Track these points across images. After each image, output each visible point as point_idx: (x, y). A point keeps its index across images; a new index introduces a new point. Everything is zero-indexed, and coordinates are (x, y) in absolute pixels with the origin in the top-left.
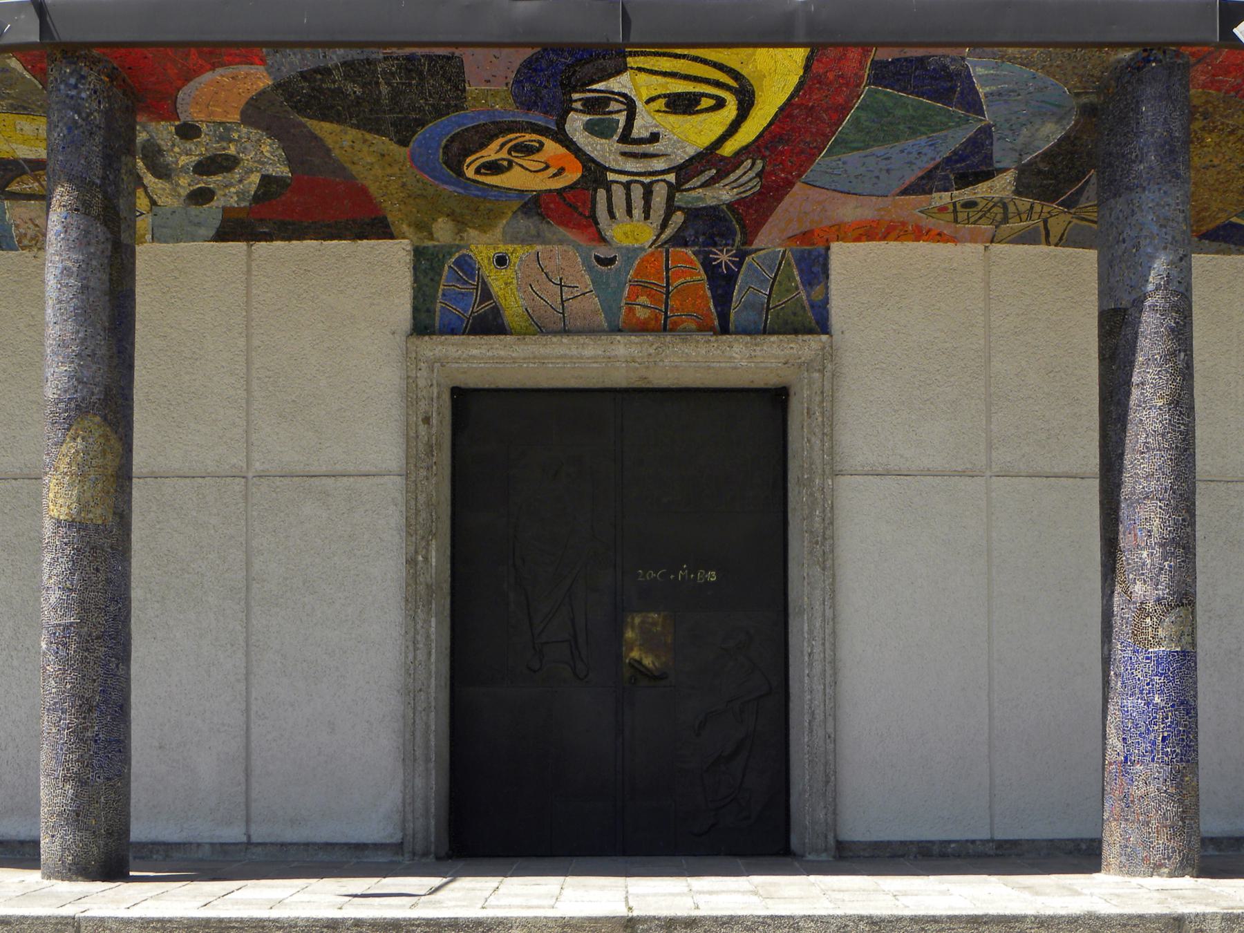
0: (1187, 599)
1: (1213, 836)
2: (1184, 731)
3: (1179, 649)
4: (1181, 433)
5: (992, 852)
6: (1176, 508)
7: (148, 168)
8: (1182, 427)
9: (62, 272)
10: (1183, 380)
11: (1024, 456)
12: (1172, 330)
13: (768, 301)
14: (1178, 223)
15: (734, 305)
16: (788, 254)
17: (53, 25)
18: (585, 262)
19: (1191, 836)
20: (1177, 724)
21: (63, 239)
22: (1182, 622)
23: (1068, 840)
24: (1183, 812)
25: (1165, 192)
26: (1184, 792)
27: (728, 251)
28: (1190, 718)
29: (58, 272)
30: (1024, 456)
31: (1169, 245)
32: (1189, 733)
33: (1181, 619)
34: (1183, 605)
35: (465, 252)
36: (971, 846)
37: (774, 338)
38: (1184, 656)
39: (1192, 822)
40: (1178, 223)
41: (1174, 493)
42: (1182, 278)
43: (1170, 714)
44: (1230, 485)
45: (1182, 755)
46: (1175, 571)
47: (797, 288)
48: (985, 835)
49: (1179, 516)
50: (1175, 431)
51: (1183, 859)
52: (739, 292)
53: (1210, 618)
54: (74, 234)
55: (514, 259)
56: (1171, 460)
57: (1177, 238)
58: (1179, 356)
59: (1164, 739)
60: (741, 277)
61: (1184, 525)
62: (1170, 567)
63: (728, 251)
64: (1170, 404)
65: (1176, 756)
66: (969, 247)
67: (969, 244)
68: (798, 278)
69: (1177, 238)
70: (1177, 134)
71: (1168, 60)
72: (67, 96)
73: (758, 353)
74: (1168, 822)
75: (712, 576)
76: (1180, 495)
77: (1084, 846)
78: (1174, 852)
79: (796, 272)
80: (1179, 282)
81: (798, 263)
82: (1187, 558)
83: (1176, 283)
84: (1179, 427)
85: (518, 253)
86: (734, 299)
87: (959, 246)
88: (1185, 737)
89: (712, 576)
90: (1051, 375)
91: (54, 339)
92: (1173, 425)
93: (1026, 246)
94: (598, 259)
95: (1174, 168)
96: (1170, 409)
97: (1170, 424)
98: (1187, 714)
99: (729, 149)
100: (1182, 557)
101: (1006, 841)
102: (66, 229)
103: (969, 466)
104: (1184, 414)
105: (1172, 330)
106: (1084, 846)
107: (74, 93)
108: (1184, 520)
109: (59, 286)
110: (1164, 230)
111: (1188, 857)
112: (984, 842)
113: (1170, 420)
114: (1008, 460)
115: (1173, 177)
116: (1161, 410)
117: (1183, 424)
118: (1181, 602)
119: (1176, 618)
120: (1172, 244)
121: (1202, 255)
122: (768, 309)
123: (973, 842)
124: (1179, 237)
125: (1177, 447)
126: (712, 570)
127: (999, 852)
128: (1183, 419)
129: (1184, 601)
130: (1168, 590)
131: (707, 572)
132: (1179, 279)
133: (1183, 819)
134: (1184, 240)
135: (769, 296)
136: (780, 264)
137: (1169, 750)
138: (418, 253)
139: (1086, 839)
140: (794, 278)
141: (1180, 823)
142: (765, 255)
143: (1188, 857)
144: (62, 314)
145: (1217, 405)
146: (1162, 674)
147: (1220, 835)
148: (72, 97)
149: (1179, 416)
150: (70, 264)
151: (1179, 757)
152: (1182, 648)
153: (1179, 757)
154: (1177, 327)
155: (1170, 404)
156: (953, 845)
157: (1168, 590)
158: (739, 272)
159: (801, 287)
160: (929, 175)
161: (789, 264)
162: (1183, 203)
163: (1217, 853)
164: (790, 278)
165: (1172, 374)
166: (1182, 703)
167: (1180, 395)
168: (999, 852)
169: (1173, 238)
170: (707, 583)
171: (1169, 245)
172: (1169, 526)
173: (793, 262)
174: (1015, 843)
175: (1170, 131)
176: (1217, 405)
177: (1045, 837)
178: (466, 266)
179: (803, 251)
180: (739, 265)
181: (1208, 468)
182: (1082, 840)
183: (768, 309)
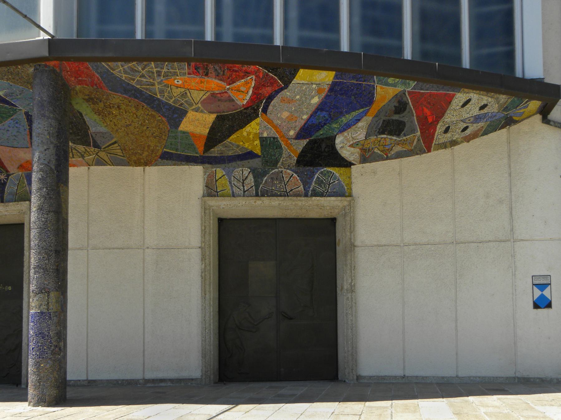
0: (44, 290)
1: (170, 378)
2: (41, 345)
3: (39, 311)
4: (42, 221)
5: (87, 384)
6: (39, 253)
8: (43, 219)
10: (45, 200)
11: (101, 242)
12: (40, 179)
13: (17, 191)
14: (44, 135)
15: (5, 193)
16: (23, 175)
17: (105, 161)
19: (44, 389)
20: (37, 342)
22: (41, 300)
23: (114, 380)
24: (39, 379)
25: (39, 123)
26: (41, 371)
27: (4, 175)
28: (45, 340)
30: (101, 242)
31: (40, 145)
32: (44, 346)
33: (41, 299)
34: (42, 293)
36: (79, 382)
37: (11, 204)
38: (42, 314)
39: (45, 383)
40: (44, 135)
41: (39, 246)
42: (46, 158)
43: (35, 338)
44: (179, 250)
45: (40, 355)
46: (39, 279)
47: (26, 186)
48: (84, 378)
49: (41, 256)
50: (39, 221)
51: (39, 399)
52: (7, 188)
53: (171, 298)
56: (38, 233)
57: (43, 142)
58: (43, 190)
59: (33, 349)
60: (8, 183)
61: (44, 260)
62: (37, 277)
64: (38, 210)
65: (37, 356)
66: (82, 168)
67: (82, 167)
68: (26, 183)
69: (43, 142)
70: (45, 99)
71: (41, 68)
73: (8, 209)
74: (33, 384)
75: (10, 288)
76: (42, 247)
77: (120, 382)
78: (35, 396)
79: (25, 181)
80: (44, 159)
81: (26, 177)
82: (44, 273)
83: (42, 160)
84: (42, 219)
86: (6, 191)
87: (79, 168)
88: (41, 348)
89: (10, 288)
90: (111, 212)
92: (38, 219)
93: (103, 167)
95: (43, 112)
96: (38, 212)
97: (37, 218)
98: (43, 338)
100: (42, 273)
101: (92, 380)
103: (81, 246)
104: (44, 214)
105: (40, 179)
106: (120, 382)
108: (43, 258)
110: (38, 138)
111: (41, 398)
112: (83, 381)
113: (38, 217)
114: (96, 243)
115: (42, 116)
116: (35, 212)
117: (43, 218)
118: (41, 291)
119: (38, 298)
120: (41, 144)
121: (169, 167)
122: (16, 194)
123: (79, 381)
124: (44, 141)
125: (40, 227)
126: (10, 286)
127: (89, 384)
128: (44, 216)
129: (43, 291)
130: (36, 287)
131: (8, 287)
132: (44, 158)
133: (39, 382)
134: (47, 142)
135: (17, 190)
136: (20, 179)
137: (34, 353)
139: (121, 380)
140: (25, 182)
141: (38, 384)
142: (16, 175)
143: (41, 398)
145: (174, 221)
146: (33, 322)
147: (173, 378)
149: (42, 214)
151: (38, 356)
152: (41, 310)
153: (38, 356)
154: (42, 178)
155: (38, 210)
156: (72, 382)
157: (36, 287)
158: (7, 182)
159: (27, 186)
161: (23, 178)
162: (48, 127)
163: (172, 385)
164: (24, 183)
165: (39, 197)
166: (40, 334)
167: (42, 206)
168: (89, 384)
169: (42, 141)
170: (8, 291)
171: (40, 145)
172: (37, 260)
173: (24, 177)
174: (94, 381)
175: (41, 98)
176: (174, 221)
177: (106, 378)
179: (28, 173)
180: (7, 179)
181: (171, 244)
182: (119, 380)
183: (16, 194)
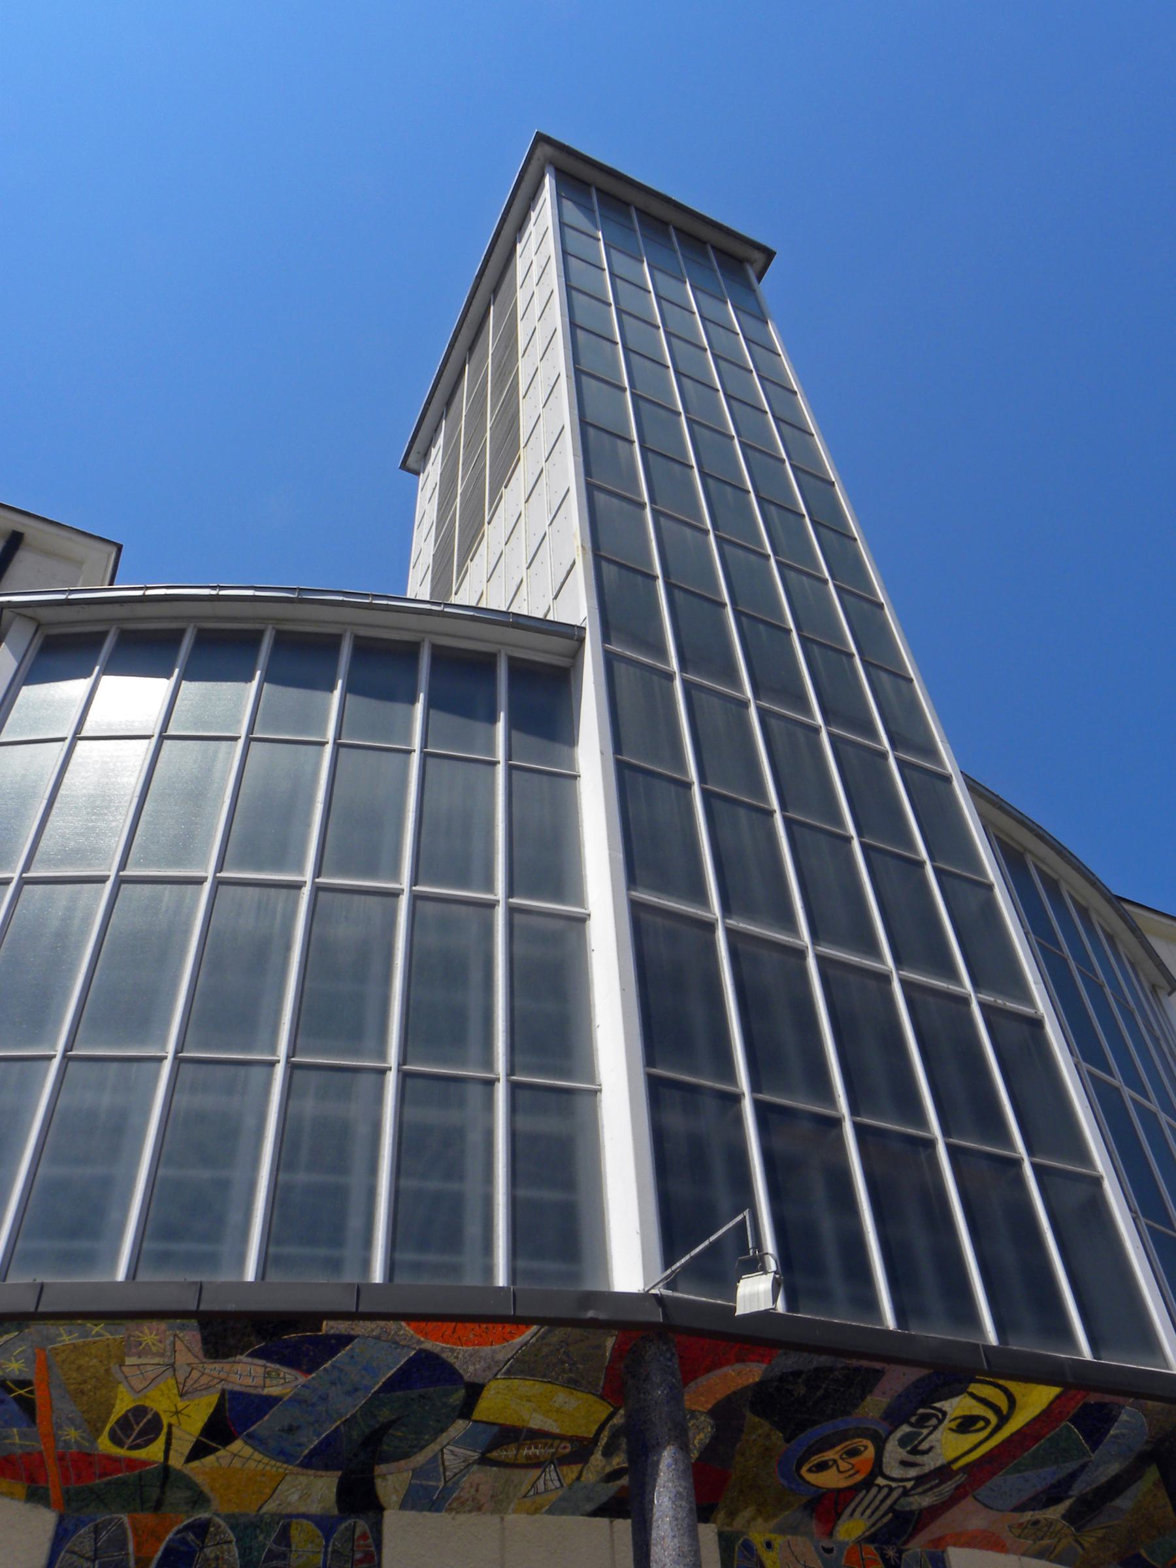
7: (604, 1447)
9: (676, 1496)
18: (816, 1548)
21: (674, 1469)
29: (672, 1495)
35: (746, 1537)
54: (682, 1467)
55: (776, 1545)
63: (893, 1549)
72: (666, 1365)
85: (778, 1540)
91: (674, 1550)
94: (823, 1548)
99: (955, 1467)
102: (676, 1461)
107: (670, 1364)
109: (674, 1506)
138: (721, 1535)
144: (679, 1530)
148: (669, 1367)
150: (681, 1490)
160: (1032, 1499)
173: (927, 1560)
178: (748, 1546)
